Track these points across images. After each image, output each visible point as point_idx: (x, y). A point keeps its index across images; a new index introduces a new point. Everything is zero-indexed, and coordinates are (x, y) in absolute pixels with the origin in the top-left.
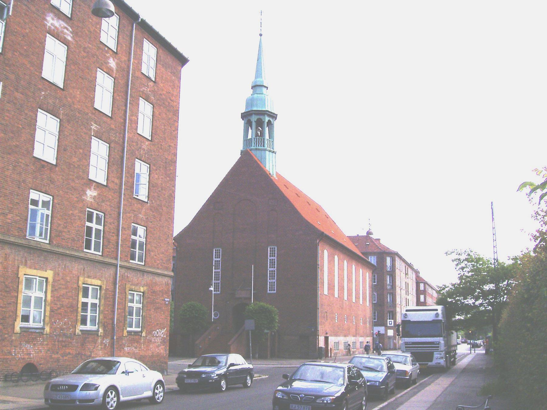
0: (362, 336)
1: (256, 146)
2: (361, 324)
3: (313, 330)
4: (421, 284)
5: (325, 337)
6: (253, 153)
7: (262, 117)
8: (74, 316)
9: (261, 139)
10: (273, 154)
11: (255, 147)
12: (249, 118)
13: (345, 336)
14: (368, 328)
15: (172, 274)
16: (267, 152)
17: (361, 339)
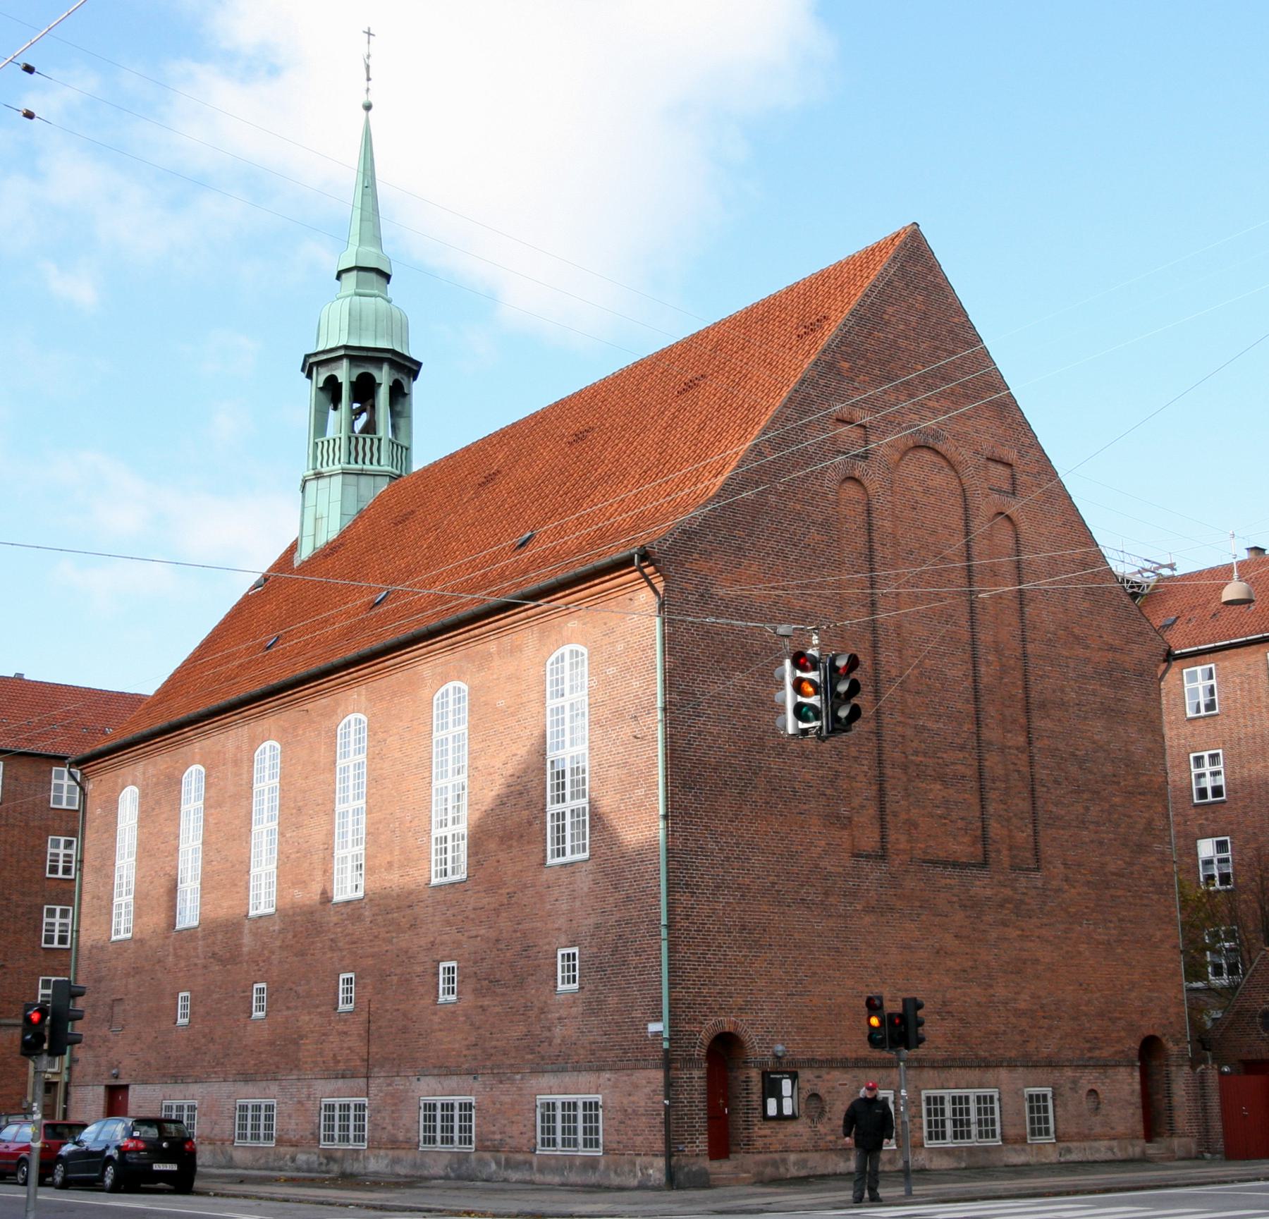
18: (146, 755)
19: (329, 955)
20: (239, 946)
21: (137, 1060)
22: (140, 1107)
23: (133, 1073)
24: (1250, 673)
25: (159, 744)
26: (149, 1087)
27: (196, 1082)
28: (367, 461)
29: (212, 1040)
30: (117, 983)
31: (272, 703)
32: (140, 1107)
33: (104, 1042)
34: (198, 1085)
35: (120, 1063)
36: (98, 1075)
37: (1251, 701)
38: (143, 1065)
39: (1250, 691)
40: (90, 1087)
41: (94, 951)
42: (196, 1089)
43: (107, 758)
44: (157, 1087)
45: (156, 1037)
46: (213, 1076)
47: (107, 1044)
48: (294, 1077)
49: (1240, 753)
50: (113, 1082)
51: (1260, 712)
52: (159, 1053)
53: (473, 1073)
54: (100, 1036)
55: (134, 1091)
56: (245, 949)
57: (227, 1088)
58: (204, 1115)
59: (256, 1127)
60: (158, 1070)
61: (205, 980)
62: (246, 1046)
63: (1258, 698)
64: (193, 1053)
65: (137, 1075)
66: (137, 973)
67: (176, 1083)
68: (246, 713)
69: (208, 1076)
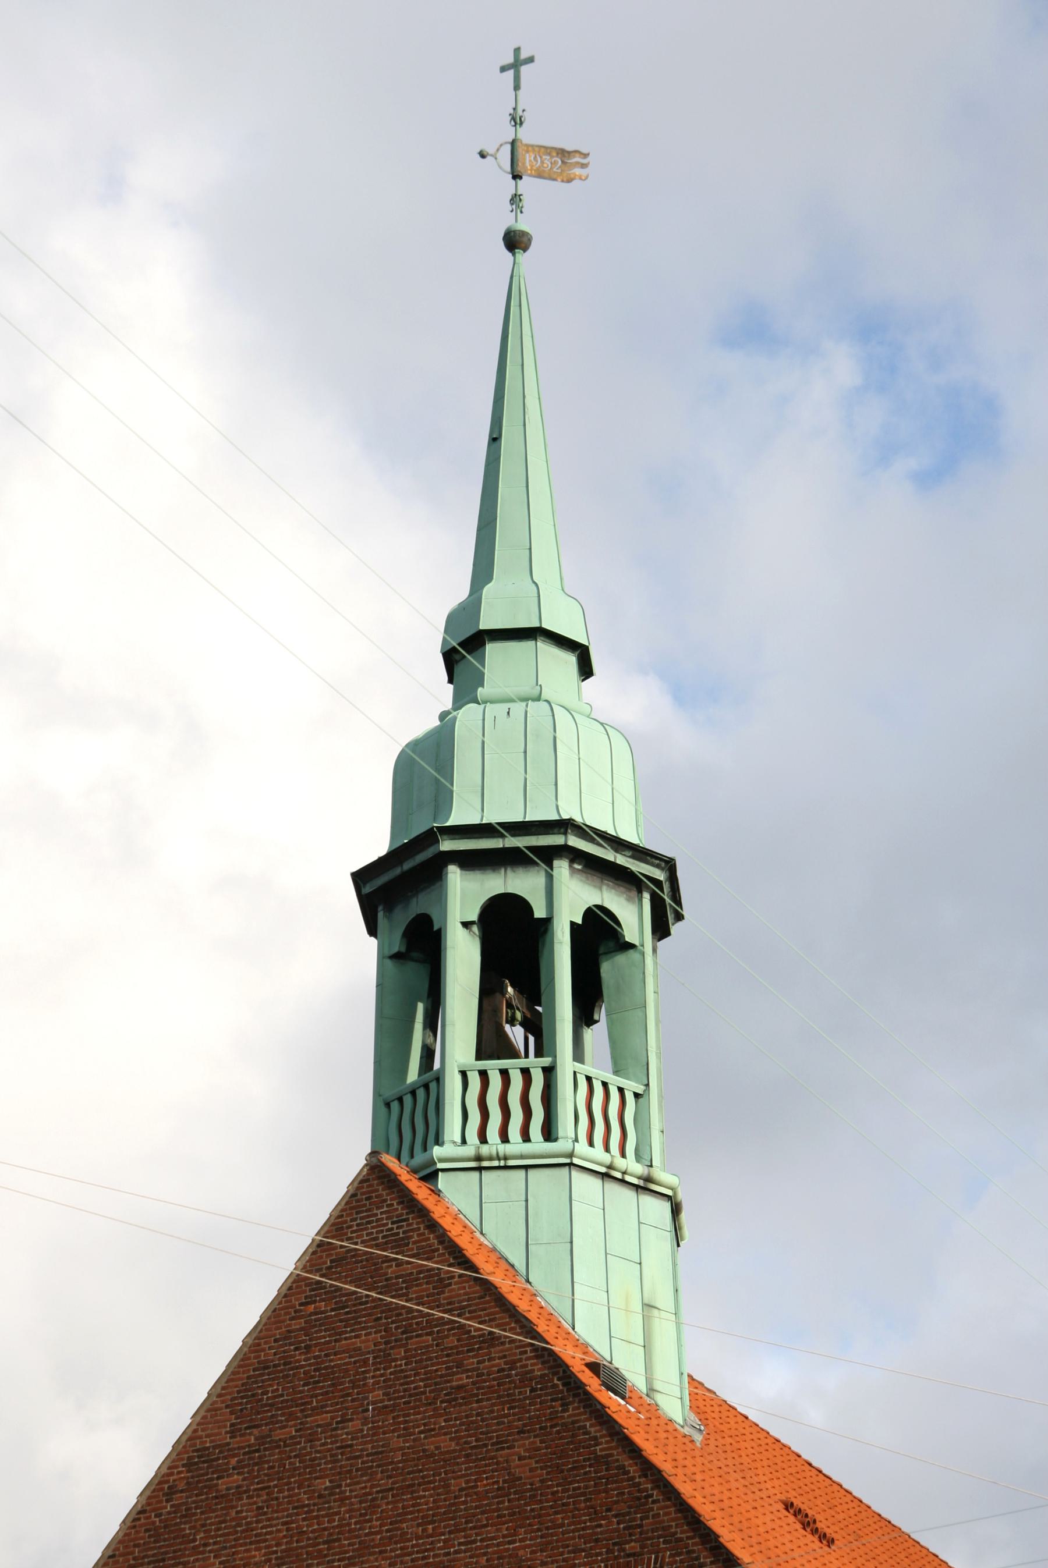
1: (483, 1139)
9: (504, 1073)
10: (647, 1200)
11: (469, 1151)
12: (419, 905)
16: (586, 1186)
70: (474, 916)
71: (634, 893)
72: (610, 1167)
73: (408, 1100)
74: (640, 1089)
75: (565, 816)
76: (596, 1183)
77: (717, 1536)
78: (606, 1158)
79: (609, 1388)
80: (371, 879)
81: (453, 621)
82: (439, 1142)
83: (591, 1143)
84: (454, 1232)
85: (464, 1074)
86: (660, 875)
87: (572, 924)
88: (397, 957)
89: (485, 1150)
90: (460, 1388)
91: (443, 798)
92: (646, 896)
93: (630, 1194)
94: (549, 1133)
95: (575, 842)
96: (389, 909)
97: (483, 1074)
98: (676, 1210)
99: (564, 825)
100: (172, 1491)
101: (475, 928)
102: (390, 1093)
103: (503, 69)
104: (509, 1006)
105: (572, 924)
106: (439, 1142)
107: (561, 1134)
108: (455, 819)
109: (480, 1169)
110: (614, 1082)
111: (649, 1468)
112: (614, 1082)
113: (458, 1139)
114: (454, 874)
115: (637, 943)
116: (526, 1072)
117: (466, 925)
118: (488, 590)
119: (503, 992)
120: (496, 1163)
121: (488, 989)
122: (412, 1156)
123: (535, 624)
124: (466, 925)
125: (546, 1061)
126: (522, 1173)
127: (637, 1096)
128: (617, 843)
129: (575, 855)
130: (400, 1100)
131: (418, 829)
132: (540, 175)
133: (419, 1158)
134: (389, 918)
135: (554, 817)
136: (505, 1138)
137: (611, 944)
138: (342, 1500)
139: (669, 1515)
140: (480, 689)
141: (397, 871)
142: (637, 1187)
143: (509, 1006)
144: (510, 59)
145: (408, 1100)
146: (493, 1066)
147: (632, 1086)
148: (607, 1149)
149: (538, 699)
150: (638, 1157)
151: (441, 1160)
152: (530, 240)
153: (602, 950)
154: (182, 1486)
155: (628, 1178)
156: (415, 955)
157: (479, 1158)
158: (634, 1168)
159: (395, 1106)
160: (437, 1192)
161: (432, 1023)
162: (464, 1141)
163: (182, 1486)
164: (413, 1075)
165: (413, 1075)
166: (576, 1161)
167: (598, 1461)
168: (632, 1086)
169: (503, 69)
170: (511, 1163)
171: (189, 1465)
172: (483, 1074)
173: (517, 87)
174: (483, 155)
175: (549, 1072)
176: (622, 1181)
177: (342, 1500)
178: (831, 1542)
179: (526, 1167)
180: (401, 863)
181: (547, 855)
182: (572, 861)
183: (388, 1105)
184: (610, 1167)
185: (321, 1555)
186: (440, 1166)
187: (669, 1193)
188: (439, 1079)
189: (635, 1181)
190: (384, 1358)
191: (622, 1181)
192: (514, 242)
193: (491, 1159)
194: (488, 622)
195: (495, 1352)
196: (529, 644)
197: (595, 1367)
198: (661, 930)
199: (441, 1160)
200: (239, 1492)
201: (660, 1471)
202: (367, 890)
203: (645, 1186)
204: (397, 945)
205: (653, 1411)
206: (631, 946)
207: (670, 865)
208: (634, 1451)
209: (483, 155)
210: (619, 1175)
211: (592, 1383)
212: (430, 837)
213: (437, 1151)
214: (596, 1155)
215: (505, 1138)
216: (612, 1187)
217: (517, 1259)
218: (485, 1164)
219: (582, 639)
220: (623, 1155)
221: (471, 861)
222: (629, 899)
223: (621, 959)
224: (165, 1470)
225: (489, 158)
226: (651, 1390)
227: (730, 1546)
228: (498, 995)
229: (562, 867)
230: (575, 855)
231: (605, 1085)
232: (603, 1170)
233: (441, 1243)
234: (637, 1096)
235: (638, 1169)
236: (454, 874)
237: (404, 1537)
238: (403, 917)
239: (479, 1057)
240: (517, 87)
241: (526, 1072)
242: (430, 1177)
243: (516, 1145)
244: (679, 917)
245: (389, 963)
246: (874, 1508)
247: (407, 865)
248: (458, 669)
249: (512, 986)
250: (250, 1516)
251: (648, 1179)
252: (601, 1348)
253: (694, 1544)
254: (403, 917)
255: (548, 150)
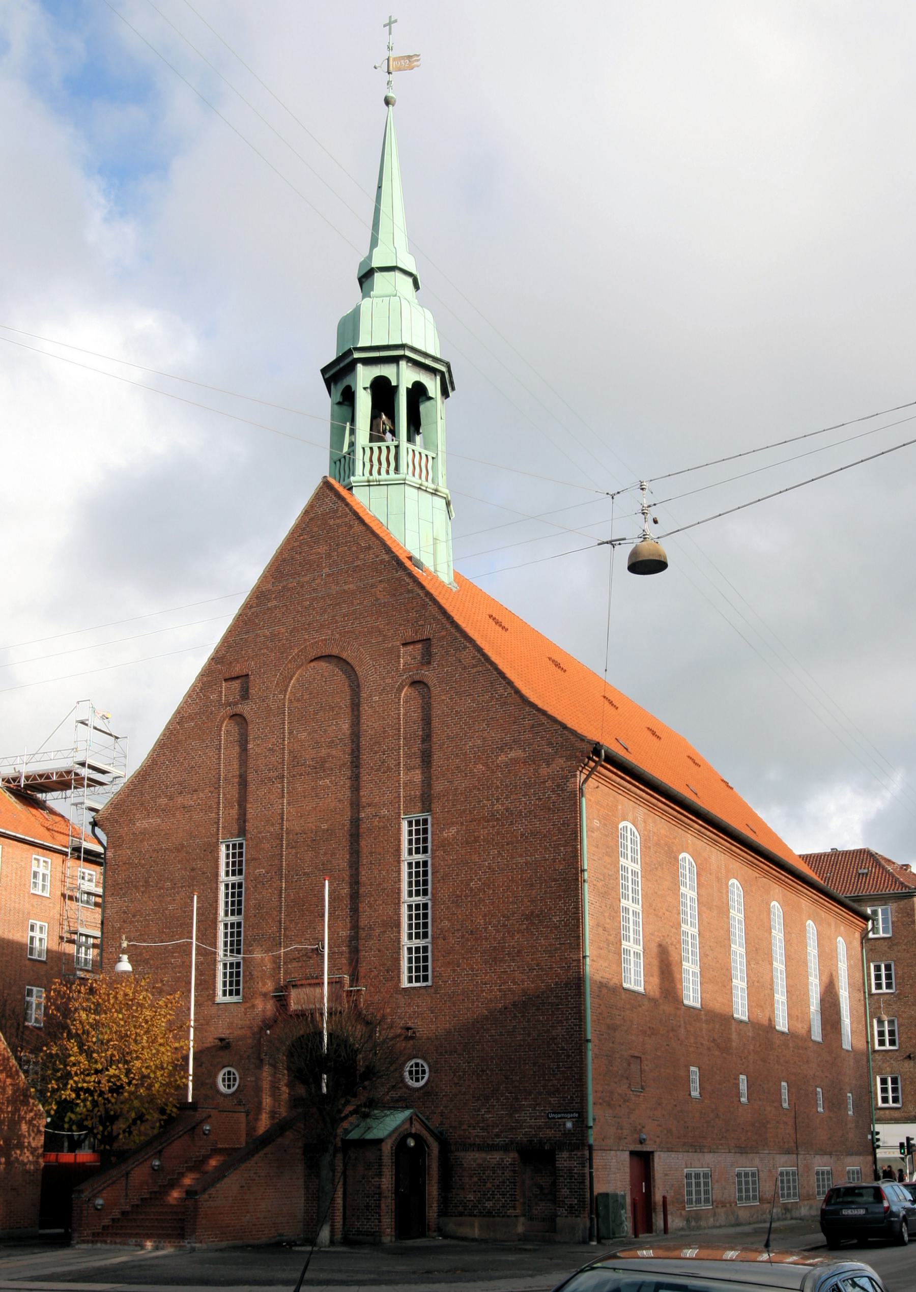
0: (824, 1153)
1: (371, 474)
2: (820, 1109)
3: (569, 1125)
4: (293, 1006)
5: (632, 1153)
6: (361, 498)
7: (388, 371)
8: (100, 997)
9: (380, 448)
10: (435, 498)
11: (365, 478)
12: (346, 382)
13: (742, 1150)
14: (851, 1125)
15: (100, 891)
16: (411, 492)
17: (821, 1164)
18: (651, 807)
19: (776, 1067)
20: (730, 1040)
21: (660, 1126)
22: (666, 1175)
23: (658, 1140)
24: (22, 864)
25: (660, 804)
26: (673, 1155)
27: (710, 1152)
28: (383, 471)
29: (717, 1116)
30: (634, 1038)
31: (749, 856)
32: (666, 1175)
33: (625, 1101)
34: (711, 1155)
35: (643, 1127)
36: (620, 1139)
37: (20, 885)
38: (665, 1132)
39: (21, 877)
40: (613, 1152)
41: (605, 991)
42: (709, 1158)
43: (628, 778)
44: (680, 1155)
45: (676, 1106)
46: (720, 1147)
47: (628, 1104)
48: (767, 1152)
49: (9, 921)
50: (639, 1148)
51: (24, 896)
52: (678, 1122)
53: (831, 1154)
54: (619, 1094)
55: (660, 1158)
56: (734, 1044)
57: (730, 1158)
58: (717, 1181)
59: (698, 1193)
60: (679, 1138)
61: (709, 1060)
62: (739, 1124)
63: (25, 884)
64: (705, 1126)
65: (661, 1142)
66: (653, 1034)
67: (696, 1152)
68: (734, 848)
69: (717, 1148)
70: (368, 385)
71: (433, 376)
72: (421, 485)
73: (343, 460)
74: (434, 456)
75: (404, 342)
76: (416, 491)
77: (453, 618)
78: (420, 482)
79: (415, 566)
80: (328, 371)
81: (361, 265)
82: (353, 475)
83: (414, 475)
84: (372, 525)
85: (364, 449)
86: (444, 369)
87: (407, 388)
88: (339, 403)
89: (371, 478)
90: (357, 566)
91: (356, 336)
92: (438, 378)
93: (429, 496)
94: (397, 469)
95: (408, 353)
96: (336, 384)
97: (371, 449)
98: (448, 504)
99: (402, 346)
100: (251, 607)
101: (369, 391)
102: (336, 458)
103: (385, 26)
104: (384, 423)
105: (407, 388)
106: (353, 475)
107: (401, 472)
108: (361, 344)
109: (369, 486)
110: (424, 452)
111: (428, 594)
112: (424, 452)
113: (361, 474)
114: (360, 367)
115: (434, 397)
116: (388, 448)
117: (365, 389)
118: (375, 250)
119: (381, 417)
120: (375, 483)
121: (375, 417)
122: (344, 480)
123: (395, 265)
124: (365, 389)
125: (396, 443)
126: (386, 487)
127: (433, 458)
128: (426, 355)
129: (409, 360)
130: (340, 460)
131: (346, 349)
132: (399, 69)
133: (347, 481)
134: (336, 388)
135: (400, 343)
136: (379, 473)
137: (424, 398)
138: (314, 609)
139: (434, 610)
140: (372, 293)
141: (338, 368)
142: (432, 493)
143: (384, 423)
144: (388, 22)
145: (343, 460)
146: (375, 445)
147: (431, 454)
148: (420, 477)
149: (396, 296)
150: (433, 482)
151: (354, 482)
152: (395, 101)
153: (420, 400)
154: (255, 605)
155: (428, 490)
156: (346, 403)
157: (369, 481)
158: (431, 486)
159: (338, 463)
160: (352, 494)
161: (352, 432)
162: (363, 475)
163: (255, 605)
164: (346, 449)
165: (346, 449)
166: (407, 482)
167: (409, 591)
168: (431, 454)
169: (385, 26)
170: (381, 483)
171: (257, 598)
172: (371, 449)
173: (390, 34)
174: (375, 68)
175: (397, 447)
176: (426, 491)
177: (314, 609)
178: (507, 630)
179: (387, 485)
180: (339, 364)
181: (395, 360)
182: (407, 362)
183: (335, 463)
184: (421, 485)
185: (306, 629)
186: (353, 484)
187: (445, 496)
188: (353, 451)
189: (431, 491)
190: (329, 556)
191: (426, 491)
192: (387, 102)
193: (373, 481)
194: (375, 264)
195: (371, 552)
196: (392, 273)
197: (410, 558)
198: (445, 393)
199: (354, 482)
200: (276, 607)
201: (432, 595)
202: (327, 376)
203: (435, 493)
204: (338, 398)
205: (435, 578)
206: (431, 398)
207: (448, 366)
208: (422, 587)
209: (375, 68)
210: (424, 488)
211: (408, 564)
212: (349, 352)
213: (352, 479)
214: (416, 480)
215: (379, 473)
216: (421, 493)
217: (384, 522)
218: (371, 483)
219: (414, 272)
220: (427, 480)
221: (367, 362)
222: (431, 379)
223: (428, 403)
224: (248, 600)
225: (379, 69)
226: (436, 571)
227: (458, 621)
228: (379, 419)
229: (403, 364)
230: (409, 360)
231: (420, 453)
232: (418, 486)
233: (351, 511)
234: (433, 458)
235: (433, 486)
236: (360, 367)
237: (337, 622)
238: (341, 387)
239: (371, 440)
240: (390, 34)
241: (388, 448)
242: (350, 489)
243: (384, 475)
244: (453, 389)
245: (335, 406)
246: (532, 626)
247: (342, 365)
248: (364, 285)
249: (385, 415)
250: (280, 616)
251: (436, 490)
252: (416, 554)
253: (444, 621)
254: (341, 387)
255: (403, 58)
